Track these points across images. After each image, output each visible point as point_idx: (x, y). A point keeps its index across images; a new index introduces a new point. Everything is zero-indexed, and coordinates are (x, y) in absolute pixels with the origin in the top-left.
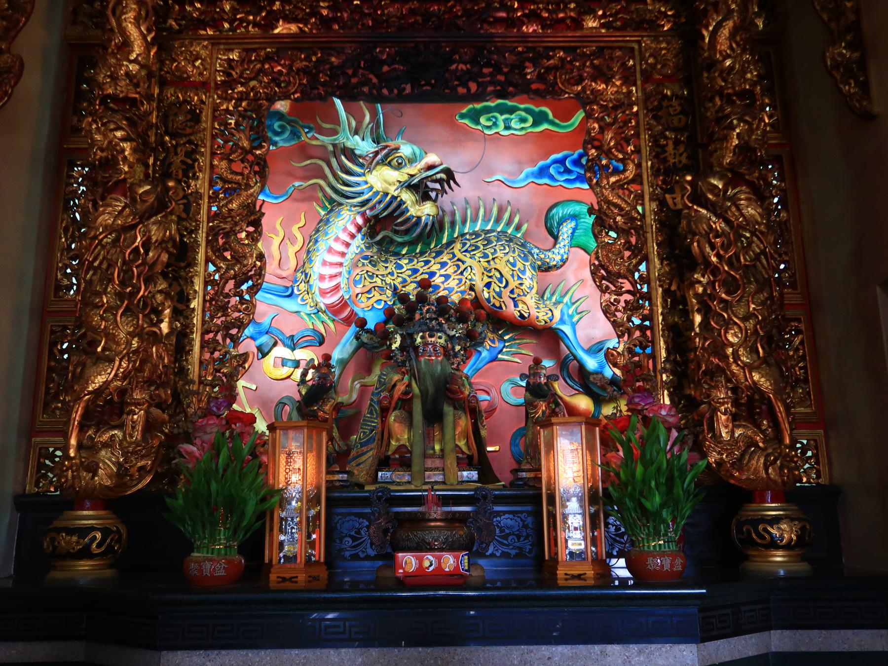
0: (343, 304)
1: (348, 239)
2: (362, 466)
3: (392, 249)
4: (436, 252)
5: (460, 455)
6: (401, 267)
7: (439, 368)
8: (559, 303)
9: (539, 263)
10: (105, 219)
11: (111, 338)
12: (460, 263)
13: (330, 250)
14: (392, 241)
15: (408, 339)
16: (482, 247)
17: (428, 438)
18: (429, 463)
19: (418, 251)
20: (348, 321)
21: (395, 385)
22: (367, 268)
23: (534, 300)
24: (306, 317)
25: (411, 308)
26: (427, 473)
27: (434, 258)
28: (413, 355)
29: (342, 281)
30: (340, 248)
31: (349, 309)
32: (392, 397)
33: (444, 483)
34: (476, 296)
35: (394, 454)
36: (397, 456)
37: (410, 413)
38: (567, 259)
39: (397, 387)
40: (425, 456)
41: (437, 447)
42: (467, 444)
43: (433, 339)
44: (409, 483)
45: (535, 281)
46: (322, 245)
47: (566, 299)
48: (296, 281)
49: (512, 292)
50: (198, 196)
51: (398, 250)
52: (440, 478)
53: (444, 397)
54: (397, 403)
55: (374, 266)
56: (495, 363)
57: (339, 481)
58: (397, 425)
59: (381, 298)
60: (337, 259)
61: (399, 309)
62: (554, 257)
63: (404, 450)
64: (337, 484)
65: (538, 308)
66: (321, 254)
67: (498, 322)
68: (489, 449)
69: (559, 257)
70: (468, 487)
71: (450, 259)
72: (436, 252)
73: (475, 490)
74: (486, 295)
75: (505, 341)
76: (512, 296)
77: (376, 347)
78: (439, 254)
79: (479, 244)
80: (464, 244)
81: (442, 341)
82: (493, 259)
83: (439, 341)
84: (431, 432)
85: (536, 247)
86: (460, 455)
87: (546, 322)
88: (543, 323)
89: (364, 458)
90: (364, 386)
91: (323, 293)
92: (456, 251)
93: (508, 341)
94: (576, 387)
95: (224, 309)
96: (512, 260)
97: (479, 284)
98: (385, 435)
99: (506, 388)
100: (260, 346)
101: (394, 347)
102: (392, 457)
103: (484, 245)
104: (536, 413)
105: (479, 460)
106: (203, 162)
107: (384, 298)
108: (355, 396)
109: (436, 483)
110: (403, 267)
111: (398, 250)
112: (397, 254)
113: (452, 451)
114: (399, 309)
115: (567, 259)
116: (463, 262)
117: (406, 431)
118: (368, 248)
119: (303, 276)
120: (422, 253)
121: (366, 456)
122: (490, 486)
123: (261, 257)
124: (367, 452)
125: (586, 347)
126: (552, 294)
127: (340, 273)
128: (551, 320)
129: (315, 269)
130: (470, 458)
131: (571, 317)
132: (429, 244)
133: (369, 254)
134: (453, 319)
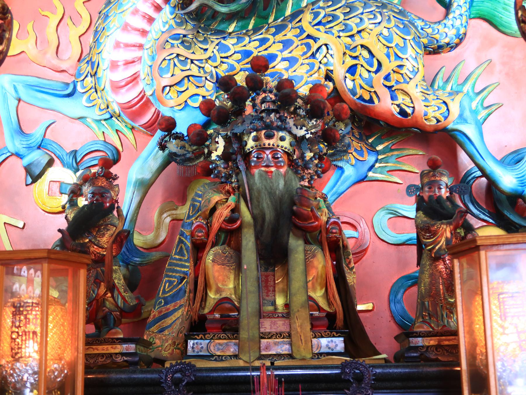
0: (144, 103)
1: (151, 12)
2: (166, 332)
3: (214, 26)
4: (276, 27)
5: (316, 313)
6: (227, 49)
7: (282, 183)
8: (457, 93)
9: (425, 41)
12: (311, 41)
13: (126, 27)
14: (215, 14)
15: (235, 141)
16: (342, 17)
17: (265, 287)
18: (267, 326)
19: (250, 27)
20: (150, 128)
21: (214, 210)
22: (176, 51)
23: (419, 89)
24: (94, 125)
25: (238, 97)
26: (264, 341)
27: (274, 35)
28: (242, 166)
29: (142, 68)
30: (140, 23)
31: (153, 110)
32: (209, 226)
33: (290, 356)
34: (335, 89)
35: (212, 312)
36: (217, 316)
37: (238, 250)
38: (465, 34)
39: (218, 212)
40: (261, 315)
41: (280, 301)
42: (327, 295)
43: (271, 142)
44: (236, 356)
45: (421, 62)
46: (115, 22)
47: (467, 87)
48: (80, 75)
49: (387, 78)
51: (222, 27)
52: (284, 349)
53: (289, 226)
54: (217, 235)
55: (188, 48)
56: (363, 184)
57: (123, 354)
58: (217, 267)
59: (198, 91)
60: (137, 39)
61: (222, 100)
62: (446, 33)
63: (228, 305)
64: (119, 359)
65: (426, 100)
66: (114, 34)
67: (371, 125)
68: (360, 307)
69: (454, 31)
70: (330, 363)
71: (297, 36)
72: (276, 27)
73: (343, 366)
74: (350, 84)
75: (378, 153)
76: (388, 84)
77: (190, 160)
78: (280, 29)
79: (338, 13)
80: (316, 15)
81: (286, 144)
82: (359, 32)
83: (281, 143)
84: (271, 278)
85: (420, 18)
86: (316, 313)
87: (438, 121)
88: (435, 121)
89: (169, 321)
90: (175, 220)
91: (116, 87)
92: (305, 24)
93: (383, 152)
94: (482, 216)
96: (385, 32)
97: (340, 72)
98: (200, 285)
99: (381, 219)
100: (29, 165)
101: (214, 156)
102: (210, 317)
103: (345, 14)
104: (436, 243)
105: (343, 320)
107: (202, 92)
108: (163, 235)
109: (279, 356)
110: (229, 49)
111: (222, 27)
112: (221, 33)
113: (302, 306)
114: (222, 100)
115: (465, 34)
116: (315, 39)
117: (232, 277)
118: (179, 24)
119: (89, 68)
120: (256, 30)
121: (173, 318)
122: (367, 361)
124: (175, 310)
125: (499, 158)
126: (447, 81)
127: (140, 59)
128: (446, 118)
129: (104, 55)
130: (331, 317)
131: (475, 112)
132: (266, 18)
133: (181, 31)
134: (302, 112)
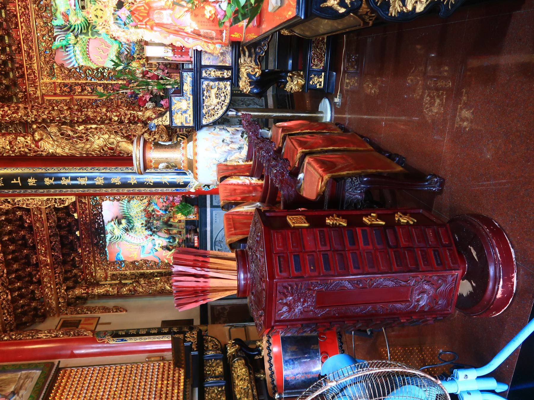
10: (141, 290)
11: (161, 287)
29: (141, 237)
46: (133, 242)
50: (130, 273)
95: (152, 266)
106: (123, 272)
123: (141, 260)
